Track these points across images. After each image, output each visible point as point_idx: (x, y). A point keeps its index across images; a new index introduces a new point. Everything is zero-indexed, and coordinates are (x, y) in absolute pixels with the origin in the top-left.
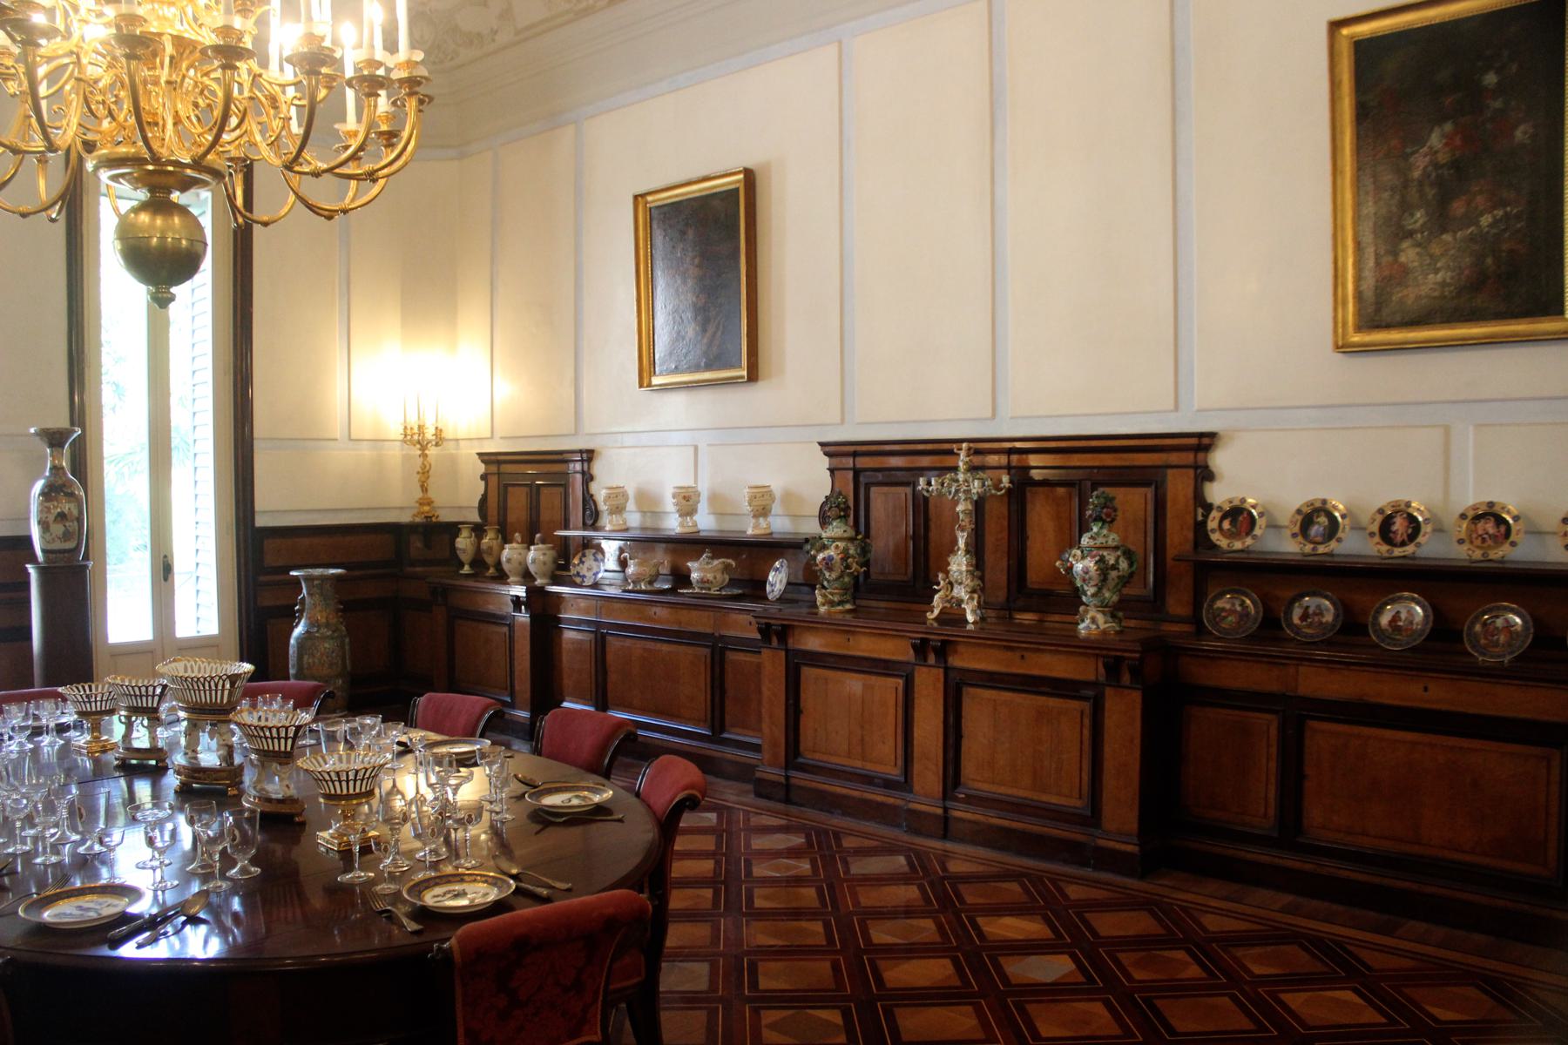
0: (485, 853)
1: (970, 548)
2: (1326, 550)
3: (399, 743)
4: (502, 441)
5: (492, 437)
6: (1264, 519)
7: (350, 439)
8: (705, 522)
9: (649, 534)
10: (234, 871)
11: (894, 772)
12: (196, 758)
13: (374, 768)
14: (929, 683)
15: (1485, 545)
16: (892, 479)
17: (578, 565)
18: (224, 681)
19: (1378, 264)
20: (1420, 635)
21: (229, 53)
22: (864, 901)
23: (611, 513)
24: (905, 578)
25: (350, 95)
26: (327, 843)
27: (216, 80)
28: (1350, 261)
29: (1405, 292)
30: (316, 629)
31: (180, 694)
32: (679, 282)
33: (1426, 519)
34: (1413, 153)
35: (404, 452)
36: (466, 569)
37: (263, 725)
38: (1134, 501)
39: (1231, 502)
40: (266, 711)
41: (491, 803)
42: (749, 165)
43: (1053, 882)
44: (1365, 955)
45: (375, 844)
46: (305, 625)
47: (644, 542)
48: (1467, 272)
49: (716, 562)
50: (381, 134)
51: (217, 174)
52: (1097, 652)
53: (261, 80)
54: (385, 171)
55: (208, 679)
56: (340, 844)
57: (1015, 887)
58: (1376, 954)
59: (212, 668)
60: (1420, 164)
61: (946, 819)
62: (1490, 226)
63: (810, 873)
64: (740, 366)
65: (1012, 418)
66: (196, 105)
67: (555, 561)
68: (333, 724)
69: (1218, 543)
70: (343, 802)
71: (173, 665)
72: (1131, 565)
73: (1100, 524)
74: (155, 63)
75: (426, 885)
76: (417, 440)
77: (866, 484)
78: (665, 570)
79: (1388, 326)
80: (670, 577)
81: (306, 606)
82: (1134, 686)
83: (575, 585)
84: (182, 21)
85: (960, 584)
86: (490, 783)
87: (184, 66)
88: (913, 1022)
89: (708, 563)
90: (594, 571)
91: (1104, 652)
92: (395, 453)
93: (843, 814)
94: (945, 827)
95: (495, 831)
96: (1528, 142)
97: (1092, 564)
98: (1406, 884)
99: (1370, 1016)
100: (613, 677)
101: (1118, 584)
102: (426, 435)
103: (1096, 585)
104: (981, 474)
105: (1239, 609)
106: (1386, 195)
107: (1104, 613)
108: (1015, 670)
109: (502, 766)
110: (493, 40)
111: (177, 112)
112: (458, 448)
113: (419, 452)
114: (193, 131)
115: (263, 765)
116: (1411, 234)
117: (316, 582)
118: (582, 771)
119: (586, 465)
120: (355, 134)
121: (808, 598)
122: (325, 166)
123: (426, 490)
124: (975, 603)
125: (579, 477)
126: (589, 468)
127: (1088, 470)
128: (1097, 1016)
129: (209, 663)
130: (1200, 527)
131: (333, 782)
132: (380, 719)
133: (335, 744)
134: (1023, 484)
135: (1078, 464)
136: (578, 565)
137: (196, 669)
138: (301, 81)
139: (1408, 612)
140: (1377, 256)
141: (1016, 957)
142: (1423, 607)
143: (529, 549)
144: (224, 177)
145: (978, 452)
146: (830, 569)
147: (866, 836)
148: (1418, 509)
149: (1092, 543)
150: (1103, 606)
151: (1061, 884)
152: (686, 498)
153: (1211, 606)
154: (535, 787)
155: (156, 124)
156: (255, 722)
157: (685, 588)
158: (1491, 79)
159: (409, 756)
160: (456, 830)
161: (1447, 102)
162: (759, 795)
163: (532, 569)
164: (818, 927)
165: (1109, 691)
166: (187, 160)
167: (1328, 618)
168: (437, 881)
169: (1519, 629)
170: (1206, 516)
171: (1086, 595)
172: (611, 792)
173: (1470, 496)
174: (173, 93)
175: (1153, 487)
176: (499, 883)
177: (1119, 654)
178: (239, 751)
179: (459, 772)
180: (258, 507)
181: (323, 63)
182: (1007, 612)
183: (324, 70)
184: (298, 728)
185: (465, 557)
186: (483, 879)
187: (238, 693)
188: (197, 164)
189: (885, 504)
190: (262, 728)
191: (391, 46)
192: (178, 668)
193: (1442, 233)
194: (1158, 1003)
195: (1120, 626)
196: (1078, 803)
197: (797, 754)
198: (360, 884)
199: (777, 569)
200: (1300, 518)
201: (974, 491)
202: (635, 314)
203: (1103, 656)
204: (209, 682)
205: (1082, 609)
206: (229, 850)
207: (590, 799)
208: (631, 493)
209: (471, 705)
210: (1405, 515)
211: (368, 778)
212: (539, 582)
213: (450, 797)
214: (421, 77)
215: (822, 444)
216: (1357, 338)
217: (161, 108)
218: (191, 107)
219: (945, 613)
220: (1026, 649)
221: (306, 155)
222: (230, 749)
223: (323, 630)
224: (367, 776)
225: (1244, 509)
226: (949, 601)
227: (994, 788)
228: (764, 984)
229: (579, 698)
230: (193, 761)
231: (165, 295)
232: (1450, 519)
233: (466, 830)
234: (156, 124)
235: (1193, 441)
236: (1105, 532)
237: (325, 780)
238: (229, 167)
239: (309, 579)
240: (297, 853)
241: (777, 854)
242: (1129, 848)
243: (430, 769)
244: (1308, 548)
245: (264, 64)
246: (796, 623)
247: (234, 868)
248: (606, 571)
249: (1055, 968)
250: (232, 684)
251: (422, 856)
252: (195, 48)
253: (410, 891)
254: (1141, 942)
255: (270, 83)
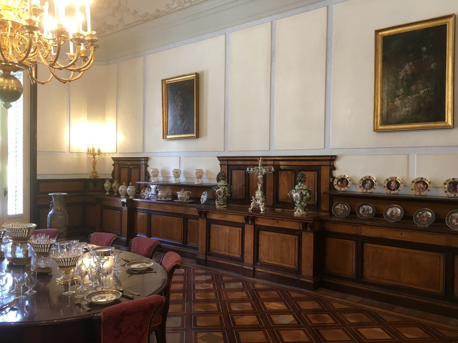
0: (112, 284)
1: (262, 189)
2: (370, 191)
3: (85, 249)
4: (120, 154)
5: (116, 153)
6: (351, 182)
7: (70, 152)
8: (182, 180)
9: (165, 183)
10: (27, 292)
11: (238, 256)
12: (15, 255)
13: (77, 257)
14: (249, 229)
15: (420, 191)
16: (239, 168)
17: (143, 192)
18: (26, 230)
19: (388, 105)
20: (400, 218)
21: (31, 28)
22: (229, 297)
23: (154, 176)
24: (242, 198)
25: (71, 44)
26: (59, 282)
27: (26, 36)
28: (379, 104)
29: (396, 114)
30: (56, 212)
31: (10, 234)
32: (175, 107)
33: (402, 183)
34: (400, 71)
35: (88, 157)
36: (107, 193)
37: (36, 244)
38: (311, 176)
39: (341, 176)
40: (40, 239)
41: (114, 267)
42: (197, 71)
43: (287, 291)
44: (384, 317)
45: (76, 282)
46: (53, 211)
47: (163, 186)
48: (415, 108)
49: (185, 192)
50: (82, 57)
51: (27, 67)
52: (300, 221)
53: (41, 37)
54: (83, 69)
55: (20, 229)
56: (64, 282)
57: (275, 293)
58: (388, 316)
59: (22, 225)
60: (402, 74)
61: (254, 271)
62: (423, 94)
63: (213, 288)
64: (193, 133)
65: (275, 150)
66: (19, 44)
67: (136, 191)
68: (63, 243)
69: (337, 189)
70: (66, 268)
71: (8, 224)
72: (310, 195)
73: (301, 182)
74: (5, 29)
75: (92, 295)
76: (92, 153)
77: (231, 169)
78: (170, 194)
79: (390, 124)
80: (171, 196)
81: (54, 205)
82: (311, 231)
83: (141, 198)
84: (14, 16)
85: (259, 200)
86: (114, 261)
87: (15, 31)
88: (244, 336)
89: (183, 192)
90: (148, 194)
91: (302, 221)
92: (85, 156)
93: (223, 269)
94: (254, 274)
95: (115, 277)
96: (435, 68)
97: (298, 195)
98: (397, 295)
99: (386, 336)
100: (153, 227)
101: (306, 200)
102: (95, 152)
103: (300, 201)
104: (265, 167)
105: (343, 208)
106: (391, 84)
107: (302, 209)
108: (275, 226)
109: (118, 255)
110: (117, 28)
111: (13, 46)
112: (105, 156)
113: (93, 157)
114: (18, 52)
115: (38, 257)
116: (398, 96)
117: (57, 197)
118: (143, 257)
119: (146, 162)
120: (74, 57)
121: (213, 203)
122: (63, 66)
123: (95, 169)
124: (263, 205)
125: (144, 165)
126: (147, 163)
127: (290, 166)
128: (302, 335)
129: (21, 224)
130: (331, 184)
131: (62, 262)
132: (78, 241)
133: (63, 249)
134: (278, 170)
135: (295, 164)
136: (143, 192)
137: (16, 226)
138: (55, 39)
139: (396, 210)
140: (388, 103)
141: (276, 315)
142: (400, 209)
143: (128, 187)
144: (29, 68)
145: (264, 160)
146: (220, 195)
147: (231, 276)
148: (399, 179)
149: (298, 188)
150: (302, 207)
151: (289, 292)
152: (177, 173)
153: (334, 208)
154: (129, 262)
155: (6, 49)
156: (36, 243)
157: (176, 200)
158: (424, 49)
159: (87, 253)
160: (102, 276)
161: (411, 56)
162: (197, 263)
163: (128, 193)
164: (215, 305)
165: (303, 233)
166: (17, 62)
167: (371, 212)
168: (96, 293)
169: (431, 216)
170: (333, 181)
171: (297, 204)
172: (153, 263)
173: (415, 176)
174: (12, 40)
175: (317, 171)
176: (117, 293)
177: (306, 221)
178: (30, 252)
179: (104, 258)
180: (38, 173)
181: (63, 33)
182: (273, 208)
183: (63, 35)
184: (51, 245)
185: (107, 190)
186: (112, 292)
187: (31, 233)
188: (20, 63)
189: (237, 176)
190: (39, 245)
191: (85, 29)
192: (10, 225)
193: (408, 96)
194: (321, 331)
195: (307, 213)
196: (294, 267)
197: (209, 250)
198: (70, 295)
199: (204, 195)
200: (362, 181)
201: (263, 172)
202: (162, 116)
203: (302, 222)
204: (21, 230)
205: (295, 208)
206: (26, 285)
207: (146, 266)
208: (160, 171)
209: (110, 236)
210: (395, 181)
211: (74, 261)
212: (131, 197)
213: (101, 266)
214: (96, 40)
215: (217, 157)
216: (380, 128)
217: (7, 44)
218: (17, 45)
219: (254, 208)
220: (279, 220)
221: (57, 62)
222: (27, 252)
223: (59, 212)
224: (74, 260)
225: (345, 179)
226: (255, 205)
227: (268, 262)
228: (199, 324)
229: (142, 233)
230: (14, 256)
231: (8, 105)
232: (409, 182)
233: (106, 277)
234: (6, 49)
235: (330, 158)
236: (302, 185)
237: (60, 261)
238: (31, 64)
239: (55, 196)
240: (49, 286)
241: (202, 282)
242: (310, 281)
243: (95, 257)
244: (365, 191)
245: (42, 32)
246: (209, 211)
247: (28, 291)
248: (152, 194)
249: (288, 319)
250: (29, 231)
251: (91, 285)
252: (19, 25)
253: (87, 297)
254: (315, 311)
255: (45, 38)
